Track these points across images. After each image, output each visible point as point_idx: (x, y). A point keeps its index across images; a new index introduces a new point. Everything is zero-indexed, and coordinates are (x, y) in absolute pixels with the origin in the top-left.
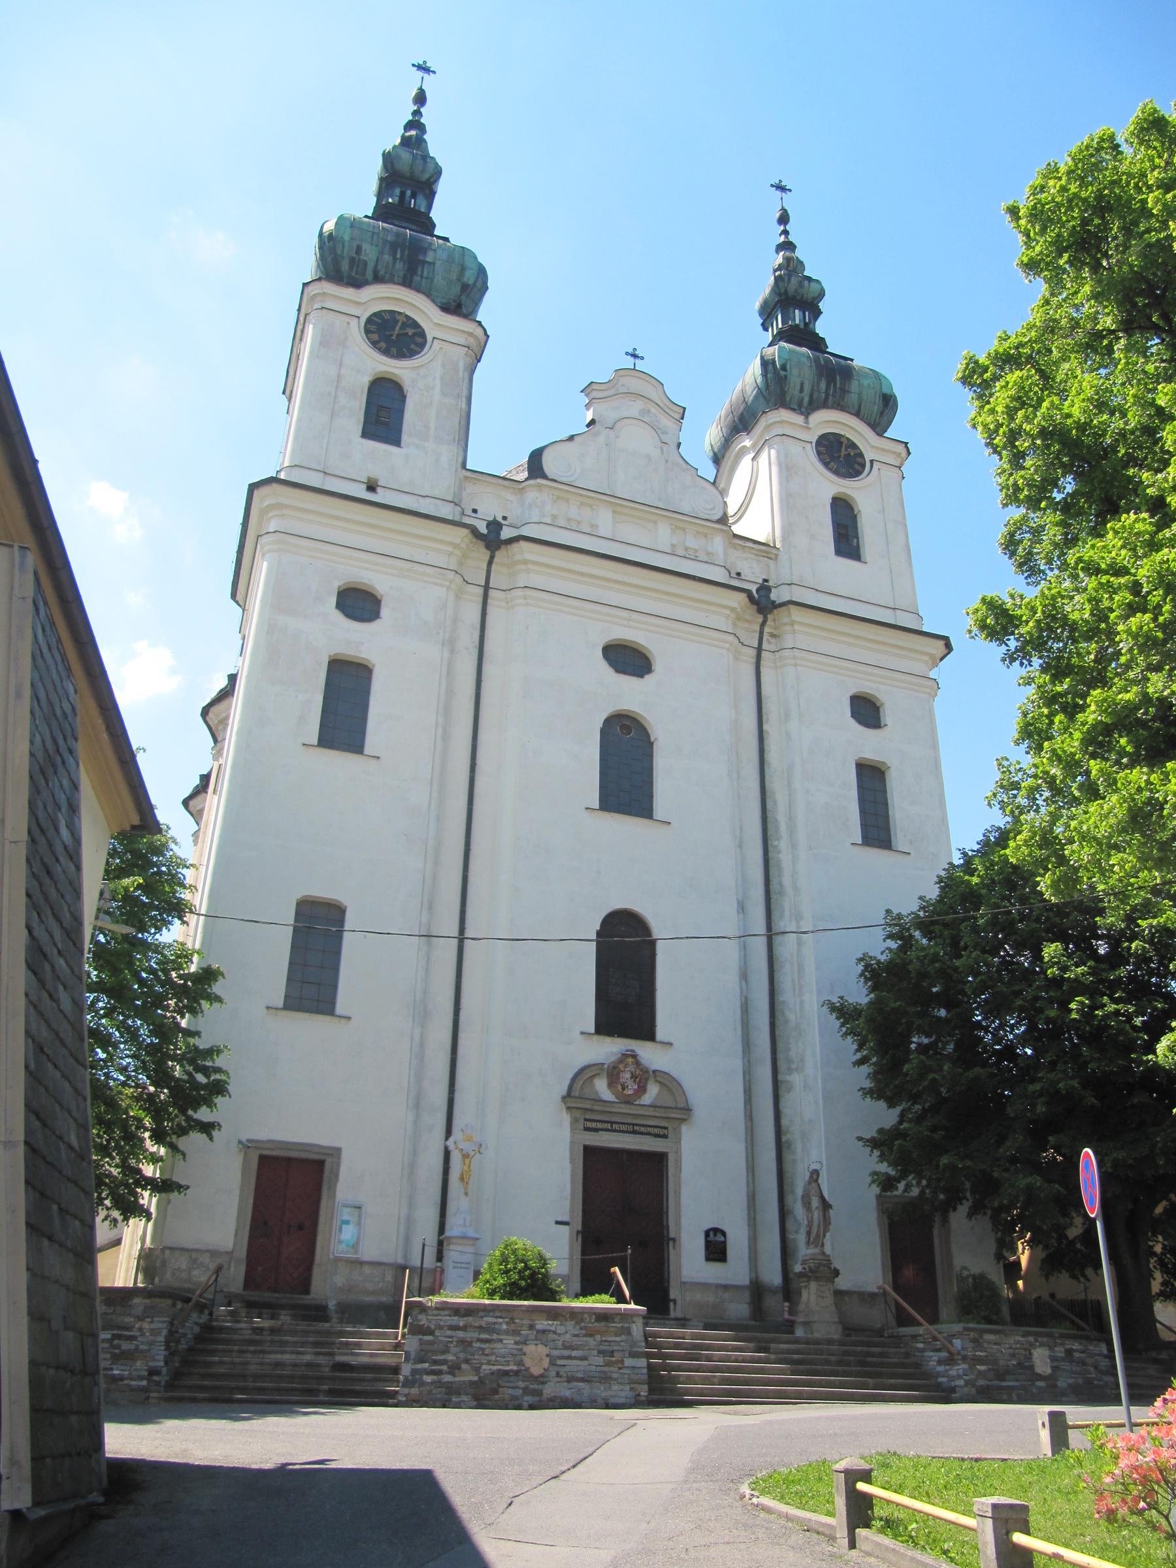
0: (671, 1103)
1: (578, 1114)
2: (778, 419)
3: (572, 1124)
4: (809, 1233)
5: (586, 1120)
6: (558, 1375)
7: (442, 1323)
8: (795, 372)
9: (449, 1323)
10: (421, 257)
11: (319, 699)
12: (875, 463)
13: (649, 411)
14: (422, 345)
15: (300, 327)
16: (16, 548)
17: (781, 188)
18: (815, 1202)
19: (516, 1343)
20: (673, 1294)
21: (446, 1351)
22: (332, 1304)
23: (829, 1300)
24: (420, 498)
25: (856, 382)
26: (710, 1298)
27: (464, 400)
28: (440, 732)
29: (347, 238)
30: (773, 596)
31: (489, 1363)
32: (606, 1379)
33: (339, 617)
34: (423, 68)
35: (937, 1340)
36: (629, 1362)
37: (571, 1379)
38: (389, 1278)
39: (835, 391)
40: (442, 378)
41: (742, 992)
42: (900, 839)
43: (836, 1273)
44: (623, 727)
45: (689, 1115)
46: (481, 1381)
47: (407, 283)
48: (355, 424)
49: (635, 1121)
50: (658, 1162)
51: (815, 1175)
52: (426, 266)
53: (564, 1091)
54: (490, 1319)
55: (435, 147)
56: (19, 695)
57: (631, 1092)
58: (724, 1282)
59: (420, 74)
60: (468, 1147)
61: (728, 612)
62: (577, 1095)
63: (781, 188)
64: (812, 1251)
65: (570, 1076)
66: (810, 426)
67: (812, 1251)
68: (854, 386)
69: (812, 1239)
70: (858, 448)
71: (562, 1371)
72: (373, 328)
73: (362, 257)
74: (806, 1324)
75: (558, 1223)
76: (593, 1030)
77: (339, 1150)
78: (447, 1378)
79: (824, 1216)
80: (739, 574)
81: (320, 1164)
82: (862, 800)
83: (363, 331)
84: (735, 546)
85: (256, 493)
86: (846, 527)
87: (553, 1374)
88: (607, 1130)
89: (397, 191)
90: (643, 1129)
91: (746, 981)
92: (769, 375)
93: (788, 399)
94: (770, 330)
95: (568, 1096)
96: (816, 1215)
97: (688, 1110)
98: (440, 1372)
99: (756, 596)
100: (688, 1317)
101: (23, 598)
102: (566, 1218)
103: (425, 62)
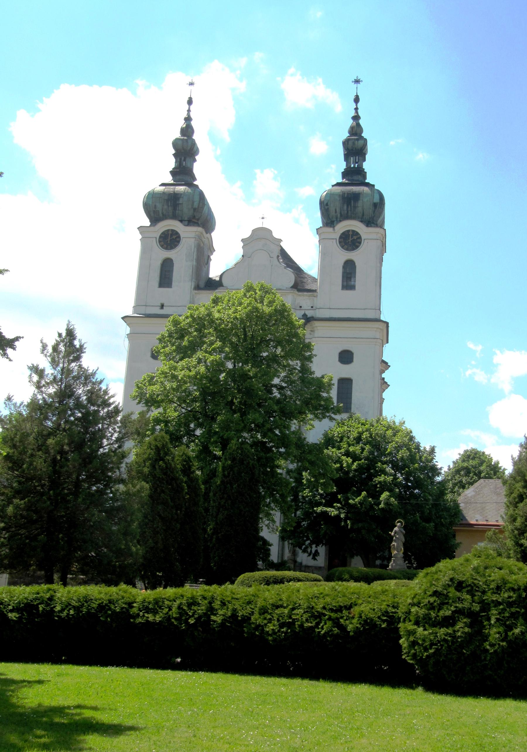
10: (178, 202)
25: (361, 201)
29: (151, 203)
47: (174, 217)
48: (157, 284)
52: (180, 205)
68: (360, 204)
70: (359, 234)
72: (357, 244)
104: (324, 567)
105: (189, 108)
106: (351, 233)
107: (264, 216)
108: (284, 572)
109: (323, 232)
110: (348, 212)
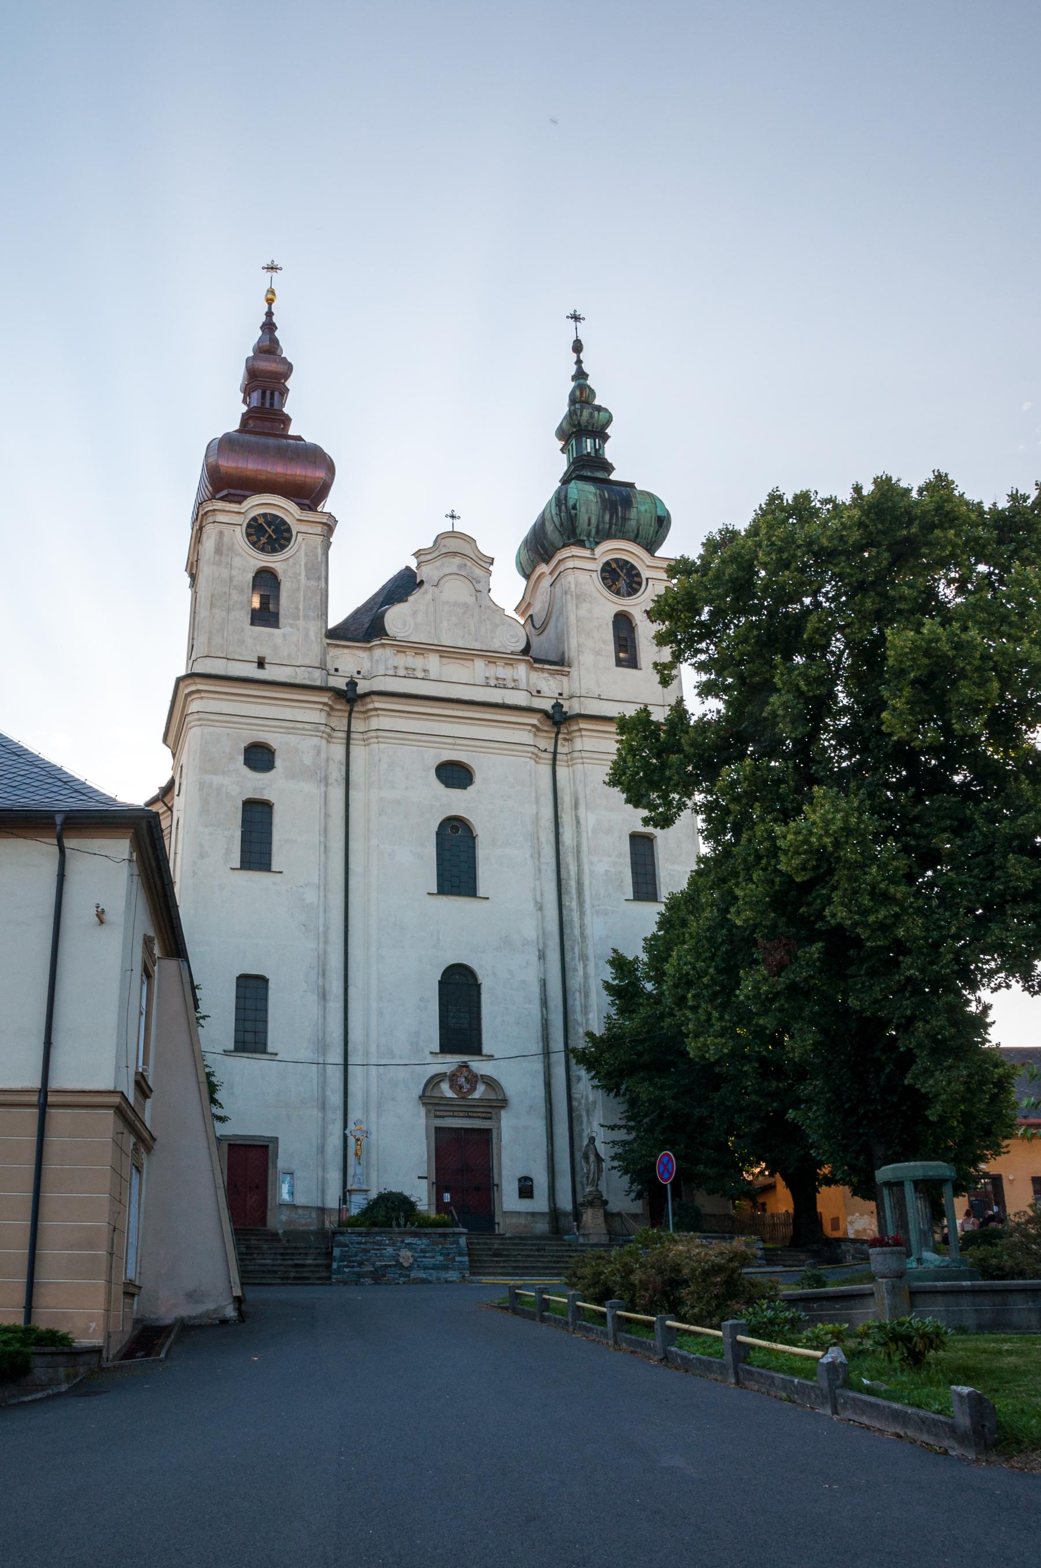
1: (430, 1107)
2: (570, 555)
6: (418, 1266)
8: (583, 510)
11: (238, 834)
13: (465, 565)
14: (289, 540)
17: (576, 318)
18: (592, 1158)
19: (394, 1250)
20: (498, 1219)
21: (356, 1255)
22: (280, 1231)
23: (601, 1220)
25: (635, 509)
26: (522, 1221)
27: (323, 580)
28: (322, 848)
31: (380, 1261)
32: (445, 1268)
33: (246, 771)
35: (369, 1251)
36: (458, 1259)
37: (426, 1268)
39: (617, 520)
40: (306, 565)
41: (542, 1016)
44: (453, 828)
46: (376, 1270)
49: (470, 1110)
50: (488, 1131)
53: (421, 1093)
55: (287, 352)
57: (465, 1090)
61: (530, 728)
63: (576, 318)
65: (424, 1081)
66: (596, 557)
68: (633, 513)
70: (636, 569)
71: (421, 1264)
72: (252, 531)
75: (419, 1178)
76: (438, 1051)
77: (277, 1138)
78: (357, 1269)
80: (539, 692)
81: (267, 1147)
83: (245, 535)
85: (182, 684)
87: (416, 1266)
88: (450, 1116)
90: (475, 1115)
91: (546, 1008)
93: (578, 532)
96: (592, 1167)
98: (353, 1267)
104: (642, 1214)
105: (578, 357)
107: (455, 513)
108: (910, 1219)
109: (573, 556)
110: (610, 527)
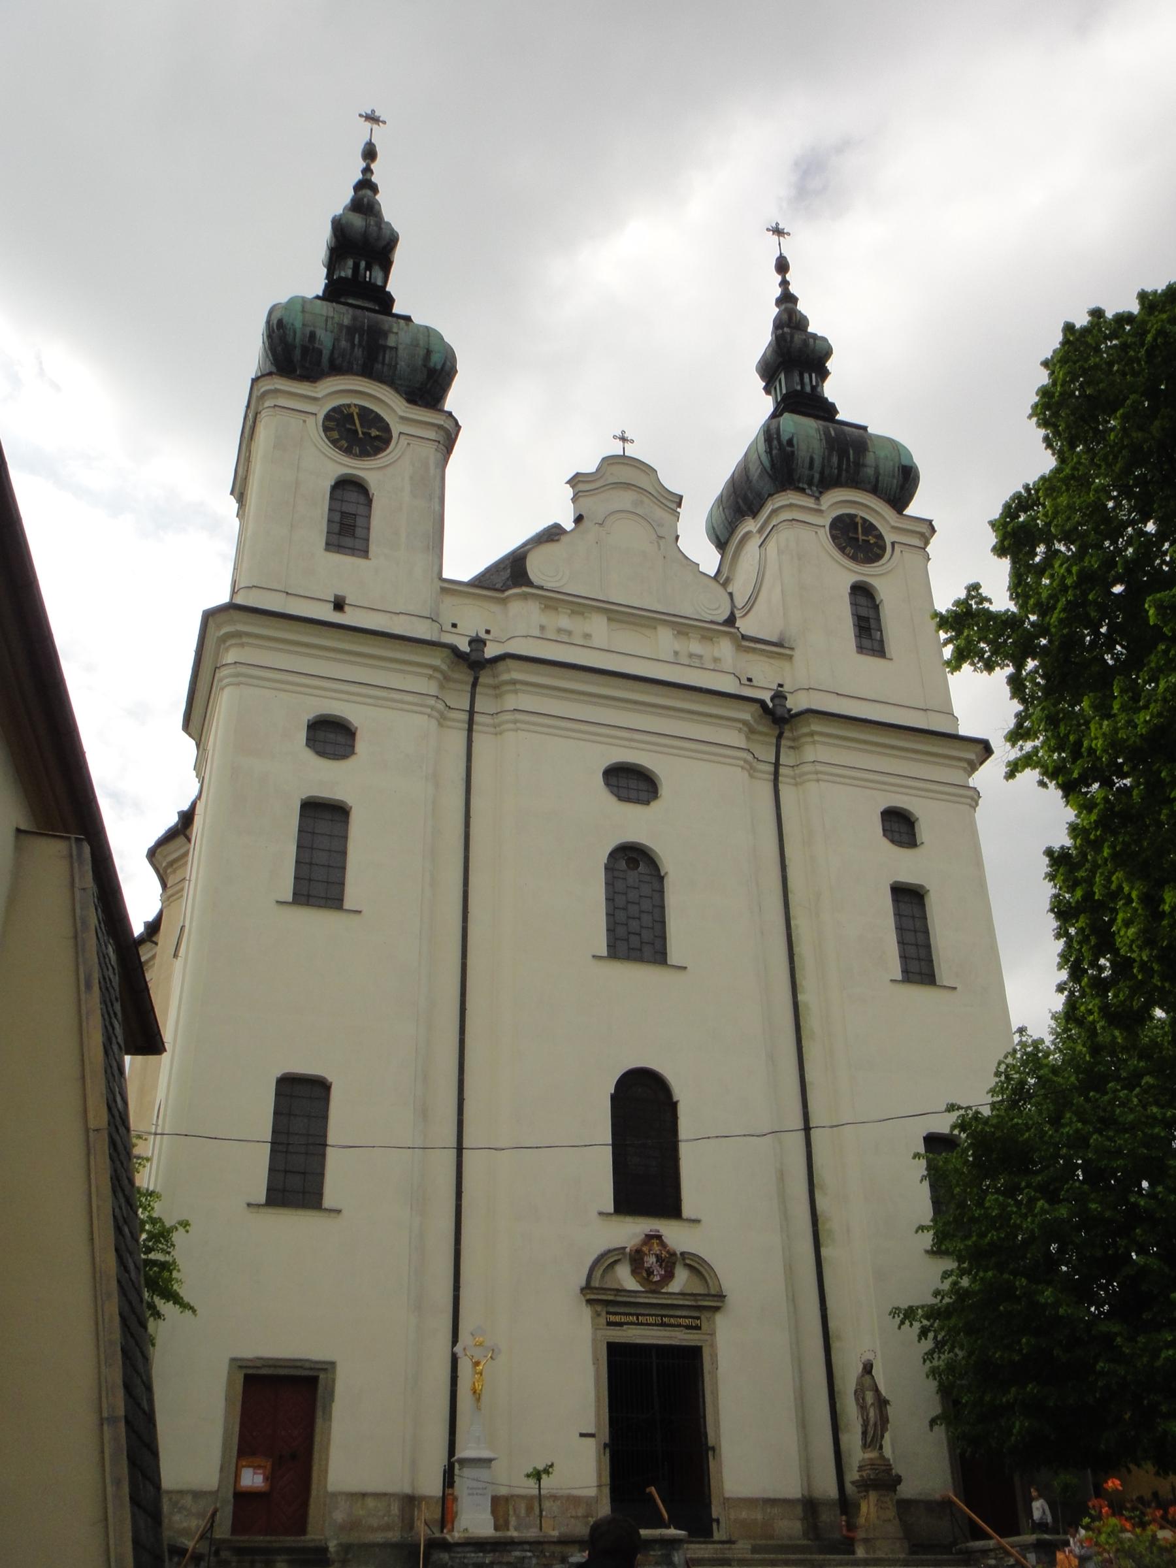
0: (700, 1290)
3: (592, 1318)
4: (864, 1433)
5: (608, 1313)
7: (466, 1561)
9: (474, 1560)
12: (896, 546)
15: (250, 423)
16: (73, 841)
22: (332, 1545)
23: (891, 1513)
24: (393, 615)
27: (437, 500)
30: (789, 704)
33: (309, 756)
34: (372, 118)
38: (395, 1509)
40: (411, 478)
42: (944, 970)
43: (898, 1480)
45: (723, 1301)
47: (368, 371)
48: (319, 537)
51: (868, 1368)
52: (388, 352)
53: (583, 1283)
54: (517, 1554)
56: (88, 986)
57: (656, 1278)
58: (771, 1495)
59: (368, 125)
60: (478, 1354)
61: (740, 725)
62: (597, 1285)
64: (872, 1455)
66: (824, 507)
67: (872, 1455)
68: (870, 459)
69: (869, 1440)
72: (332, 424)
73: (317, 345)
74: (866, 1541)
75: (582, 1435)
76: (612, 1210)
79: (881, 1412)
80: (750, 680)
82: (900, 929)
83: (321, 429)
84: (748, 650)
85: (211, 620)
86: (867, 619)
88: (632, 1324)
89: (350, 263)
90: (672, 1321)
92: (774, 452)
94: (773, 392)
95: (587, 1288)
97: (721, 1297)
99: (771, 705)
100: (733, 1539)
101: (84, 889)
102: (592, 1430)
103: (373, 111)
106: (355, 411)
